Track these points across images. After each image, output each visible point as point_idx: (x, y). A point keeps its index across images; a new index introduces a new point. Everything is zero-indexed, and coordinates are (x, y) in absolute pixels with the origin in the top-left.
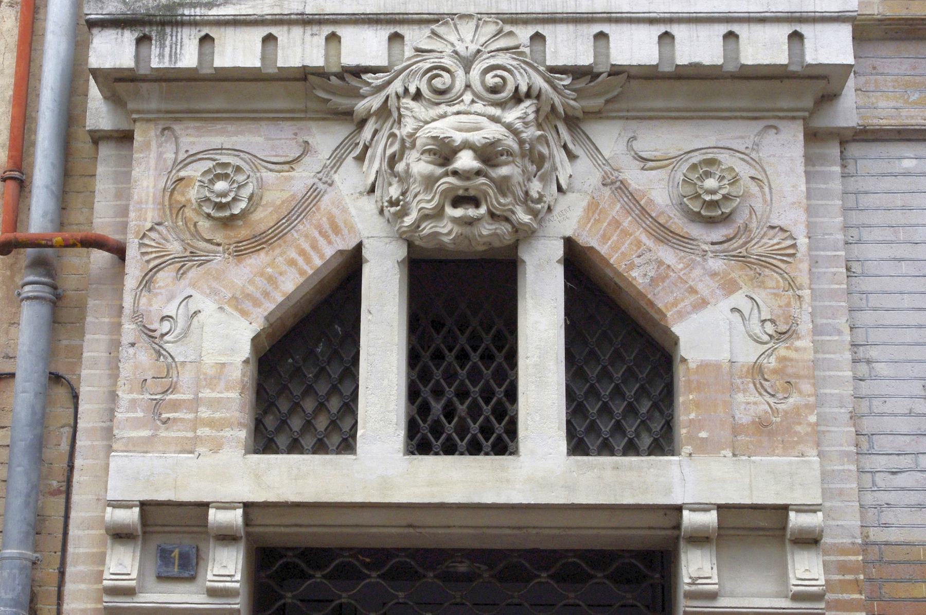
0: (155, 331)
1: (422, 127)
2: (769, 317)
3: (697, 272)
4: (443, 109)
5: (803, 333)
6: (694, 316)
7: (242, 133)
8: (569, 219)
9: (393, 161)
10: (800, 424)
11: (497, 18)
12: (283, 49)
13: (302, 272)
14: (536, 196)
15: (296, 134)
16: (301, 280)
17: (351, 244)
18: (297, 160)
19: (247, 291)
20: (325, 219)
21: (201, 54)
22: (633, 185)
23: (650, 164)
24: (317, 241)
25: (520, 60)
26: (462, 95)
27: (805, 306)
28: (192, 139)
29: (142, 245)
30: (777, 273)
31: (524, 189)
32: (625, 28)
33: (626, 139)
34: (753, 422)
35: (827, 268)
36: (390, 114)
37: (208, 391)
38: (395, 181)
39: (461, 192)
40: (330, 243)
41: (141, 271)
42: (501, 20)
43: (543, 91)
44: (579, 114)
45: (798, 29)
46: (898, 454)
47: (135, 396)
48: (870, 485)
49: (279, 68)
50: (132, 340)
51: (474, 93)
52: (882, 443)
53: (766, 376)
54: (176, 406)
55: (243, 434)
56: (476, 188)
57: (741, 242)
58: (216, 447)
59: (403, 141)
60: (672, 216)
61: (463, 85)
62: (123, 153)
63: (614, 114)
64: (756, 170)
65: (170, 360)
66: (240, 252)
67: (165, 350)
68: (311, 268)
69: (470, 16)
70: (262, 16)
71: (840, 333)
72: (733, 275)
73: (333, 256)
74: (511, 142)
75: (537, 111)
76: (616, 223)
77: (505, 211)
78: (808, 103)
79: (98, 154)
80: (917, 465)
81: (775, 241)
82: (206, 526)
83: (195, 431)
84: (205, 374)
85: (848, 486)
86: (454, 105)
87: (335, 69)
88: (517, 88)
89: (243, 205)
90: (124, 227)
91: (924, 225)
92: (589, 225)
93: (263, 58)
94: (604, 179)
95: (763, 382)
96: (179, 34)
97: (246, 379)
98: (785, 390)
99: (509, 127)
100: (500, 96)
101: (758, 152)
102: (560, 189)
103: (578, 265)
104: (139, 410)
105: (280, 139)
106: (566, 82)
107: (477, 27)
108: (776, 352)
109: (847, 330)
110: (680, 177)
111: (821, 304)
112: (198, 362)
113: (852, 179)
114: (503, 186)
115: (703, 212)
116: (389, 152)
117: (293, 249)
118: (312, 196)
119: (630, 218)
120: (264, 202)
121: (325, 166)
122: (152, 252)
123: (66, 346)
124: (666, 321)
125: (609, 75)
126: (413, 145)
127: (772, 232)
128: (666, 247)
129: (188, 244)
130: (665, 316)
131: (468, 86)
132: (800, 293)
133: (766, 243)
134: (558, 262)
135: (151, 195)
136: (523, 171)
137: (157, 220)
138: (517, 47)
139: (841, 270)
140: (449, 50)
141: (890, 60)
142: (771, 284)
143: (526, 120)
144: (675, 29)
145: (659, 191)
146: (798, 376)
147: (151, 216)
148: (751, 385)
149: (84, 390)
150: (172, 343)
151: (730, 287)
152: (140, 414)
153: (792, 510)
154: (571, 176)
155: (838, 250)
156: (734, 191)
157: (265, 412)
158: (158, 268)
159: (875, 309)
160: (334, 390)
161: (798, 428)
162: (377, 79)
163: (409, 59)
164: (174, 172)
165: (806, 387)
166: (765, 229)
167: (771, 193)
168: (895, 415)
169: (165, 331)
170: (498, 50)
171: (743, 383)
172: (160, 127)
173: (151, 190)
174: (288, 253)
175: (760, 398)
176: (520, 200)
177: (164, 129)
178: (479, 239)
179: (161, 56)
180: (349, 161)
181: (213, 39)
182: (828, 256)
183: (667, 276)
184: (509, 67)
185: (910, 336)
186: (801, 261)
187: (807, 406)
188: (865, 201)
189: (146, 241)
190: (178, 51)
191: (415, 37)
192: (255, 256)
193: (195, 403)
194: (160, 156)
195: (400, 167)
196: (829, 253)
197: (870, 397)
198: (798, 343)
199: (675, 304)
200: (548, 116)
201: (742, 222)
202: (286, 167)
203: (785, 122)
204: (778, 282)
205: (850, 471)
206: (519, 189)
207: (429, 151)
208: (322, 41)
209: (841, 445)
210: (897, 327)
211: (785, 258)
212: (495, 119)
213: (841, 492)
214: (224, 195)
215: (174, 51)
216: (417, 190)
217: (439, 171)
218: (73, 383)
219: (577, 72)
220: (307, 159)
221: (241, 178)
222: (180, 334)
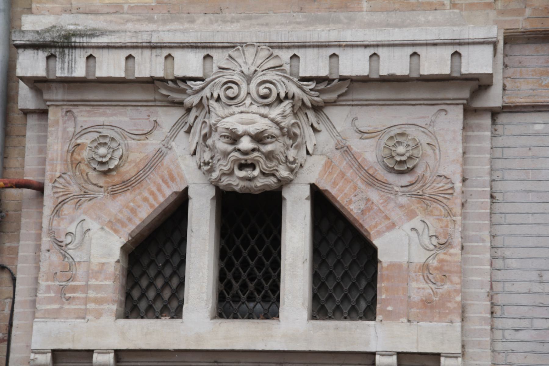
0: (62, 242)
1: (220, 120)
2: (434, 234)
3: (392, 205)
4: (234, 109)
5: (455, 245)
6: (387, 234)
7: (115, 115)
8: (313, 172)
9: (205, 137)
10: (450, 302)
13: (152, 206)
14: (291, 159)
15: (149, 116)
16: (151, 210)
17: (181, 188)
18: (149, 133)
19: (119, 218)
20: (166, 172)
21: (87, 67)
22: (355, 149)
23: (366, 135)
24: (161, 186)
27: (457, 227)
28: (85, 119)
29: (54, 187)
30: (441, 205)
31: (285, 155)
32: (349, 51)
34: (422, 300)
35: (478, 199)
36: (204, 107)
37: (94, 280)
38: (207, 149)
39: (243, 162)
40: (168, 187)
41: (54, 204)
43: (296, 95)
44: (322, 104)
45: (458, 50)
46: (520, 318)
47: (50, 283)
48: (501, 338)
50: (47, 248)
51: (253, 99)
52: (510, 311)
53: (431, 272)
54: (74, 289)
55: (114, 307)
56: (252, 159)
57: (419, 185)
58: (99, 315)
59: (211, 126)
60: (377, 169)
61: (246, 93)
62: (43, 123)
63: (344, 103)
64: (431, 138)
65: (71, 260)
66: (114, 193)
67: (68, 254)
68: (157, 203)
69: (253, 45)
70: (125, 43)
71: (483, 241)
72: (413, 207)
73: (171, 195)
74: (275, 131)
75: (293, 106)
76: (343, 174)
77: (272, 171)
78: (466, 94)
79: (26, 121)
80: (532, 326)
81: (441, 185)
82: (92, 363)
83: (86, 305)
84: (92, 270)
85: (484, 339)
87: (171, 77)
88: (278, 95)
89: (116, 162)
90: (43, 172)
91: (546, 169)
92: (326, 176)
93: (126, 70)
94: (337, 145)
95: (429, 275)
96: (73, 54)
97: (117, 272)
98: (442, 280)
99: (272, 120)
100: (266, 100)
101: (433, 127)
102: (308, 153)
103: (320, 201)
104: (52, 292)
105: (139, 119)
106: (311, 87)
107: (257, 51)
108: (437, 257)
109: (488, 239)
110: (383, 145)
111: (473, 222)
112: (89, 262)
113: (501, 138)
114: (270, 156)
115: (396, 168)
116: (203, 132)
118: (160, 154)
120: (129, 160)
121: (167, 137)
122: (60, 192)
123: (9, 247)
124: (370, 237)
125: (340, 80)
126: (216, 130)
127: (439, 179)
128: (373, 189)
129: (83, 186)
130: (369, 233)
131: (249, 93)
132: (454, 218)
133: (435, 187)
134: (307, 199)
135: (60, 155)
136: (284, 144)
137: (63, 171)
138: (281, 66)
139: (486, 200)
140: (238, 70)
141: (531, 57)
142: (436, 212)
143: (284, 115)
144: (380, 51)
145: (370, 152)
146: (450, 272)
147: (59, 169)
148: (421, 277)
149: (19, 277)
150: (73, 249)
151: (411, 215)
152: (53, 295)
153: (443, 356)
154: (315, 145)
155: (485, 187)
156: (415, 152)
157: (132, 288)
158: (63, 202)
159: (510, 224)
160: (174, 273)
161: (449, 305)
162: (196, 85)
163: (215, 74)
164: (74, 140)
165: (455, 279)
166: (435, 177)
167: (440, 154)
168: (519, 293)
169: (68, 242)
170: (268, 69)
171: (416, 275)
172: (65, 110)
173: (59, 152)
174: (143, 193)
175: (426, 286)
176: (282, 162)
177: (67, 112)
178: (255, 189)
179: (63, 68)
180: (182, 133)
181: (134, 58)
182: (478, 191)
183: (372, 209)
184: (274, 81)
185: (531, 241)
186: (456, 198)
187: (455, 290)
188: (508, 153)
189: (56, 184)
190: (73, 66)
191: (220, 58)
192: (123, 194)
193: (86, 288)
194: (65, 129)
195: (209, 142)
196: (480, 189)
197: (504, 281)
198: (452, 251)
199: (375, 227)
200: (299, 108)
201: (420, 172)
202: (143, 137)
203: (452, 107)
204: (441, 211)
205: (486, 329)
206: (281, 155)
207: (224, 136)
209: (481, 313)
210: (524, 236)
211: (446, 196)
212: (264, 116)
213: (479, 343)
214: (104, 156)
215: (70, 65)
216: (219, 157)
217: (230, 148)
218: (13, 271)
219: (319, 80)
220: (156, 132)
221: (114, 145)
222: (78, 244)
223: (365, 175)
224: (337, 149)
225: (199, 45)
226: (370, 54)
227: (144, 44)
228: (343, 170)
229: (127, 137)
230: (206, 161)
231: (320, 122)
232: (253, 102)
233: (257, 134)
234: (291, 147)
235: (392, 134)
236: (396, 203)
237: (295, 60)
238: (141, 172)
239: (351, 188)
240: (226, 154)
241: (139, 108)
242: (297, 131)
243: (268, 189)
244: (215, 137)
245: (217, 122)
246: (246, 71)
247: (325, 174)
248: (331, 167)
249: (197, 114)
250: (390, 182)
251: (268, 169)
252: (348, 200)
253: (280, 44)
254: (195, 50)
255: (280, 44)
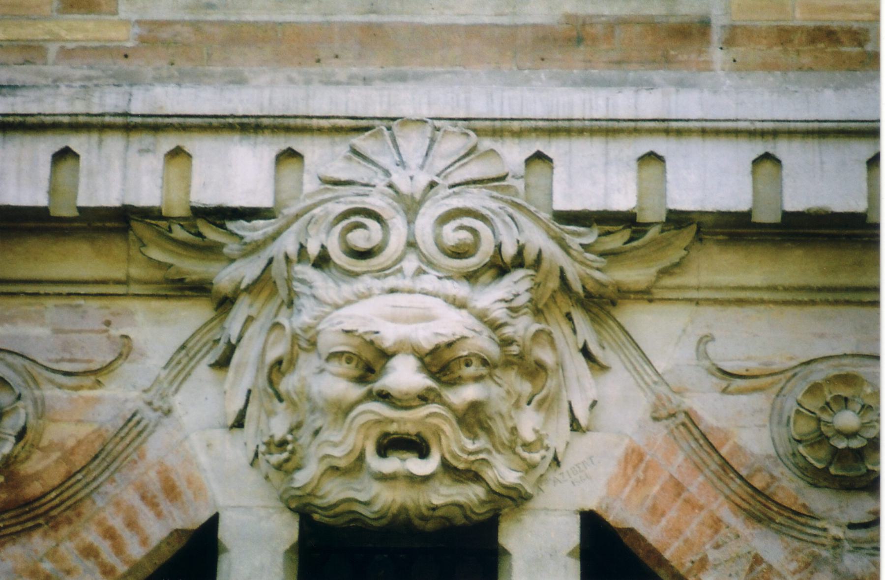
1: (328, 314)
11: (468, 128)
12: (90, 174)
15: (108, 323)
17: (204, 516)
18: (107, 368)
25: (506, 202)
26: (400, 260)
31: (510, 424)
33: (694, 340)
42: (475, 130)
43: (545, 255)
45: (181, 144)
49: (81, 209)
59: (295, 337)
61: (403, 240)
68: (125, 562)
73: (167, 541)
76: (678, 488)
77: (473, 462)
86: (386, 276)
87: (179, 211)
92: (628, 490)
93: (53, 191)
94: (655, 409)
99: (482, 317)
102: (575, 425)
106: (586, 241)
107: (433, 141)
110: (790, 406)
114: (473, 418)
115: (832, 470)
116: (272, 355)
117: (93, 528)
118: (133, 428)
119: (701, 479)
121: (157, 380)
131: (412, 244)
136: (508, 392)
138: (503, 178)
143: (514, 304)
154: (594, 404)
162: (255, 229)
170: (467, 183)
174: (84, 535)
176: (503, 444)
181: (76, 156)
184: (485, 212)
191: (322, 157)
195: (288, 384)
202: (89, 380)
208: (45, 159)
212: (460, 305)
217: (356, 391)
220: (126, 368)
223: (739, 491)
224: (656, 419)
225: (265, 121)
226: (754, 156)
227: (107, 119)
228: (676, 476)
229: (40, 380)
230: (278, 437)
231: (605, 345)
232: (424, 267)
233: (435, 351)
234: (529, 403)
235: (817, 377)
236: (836, 571)
237: (539, 167)
238: (79, 476)
239: (703, 524)
240: (344, 410)
241: (80, 301)
242: (546, 356)
243: (460, 520)
244: (307, 365)
245: (319, 318)
246: (404, 186)
247: (625, 486)
248: (643, 465)
249: (253, 312)
250: (818, 513)
251: (465, 456)
252: (696, 558)
253: (498, 124)
254: (252, 136)
255: (498, 124)
